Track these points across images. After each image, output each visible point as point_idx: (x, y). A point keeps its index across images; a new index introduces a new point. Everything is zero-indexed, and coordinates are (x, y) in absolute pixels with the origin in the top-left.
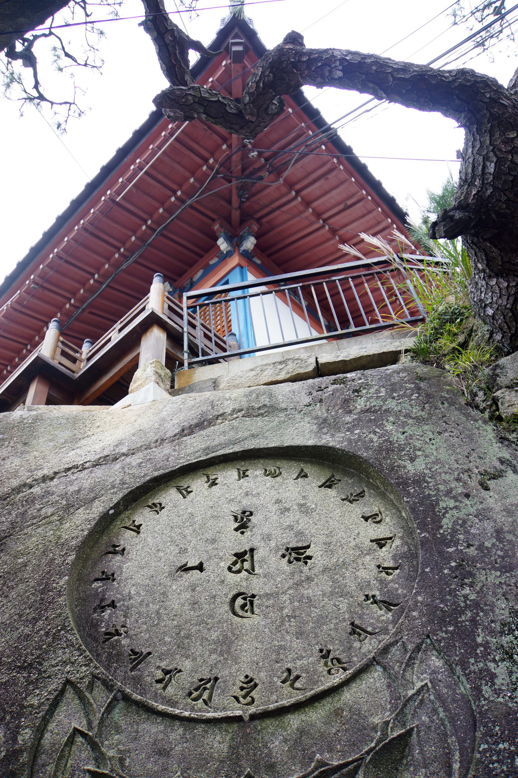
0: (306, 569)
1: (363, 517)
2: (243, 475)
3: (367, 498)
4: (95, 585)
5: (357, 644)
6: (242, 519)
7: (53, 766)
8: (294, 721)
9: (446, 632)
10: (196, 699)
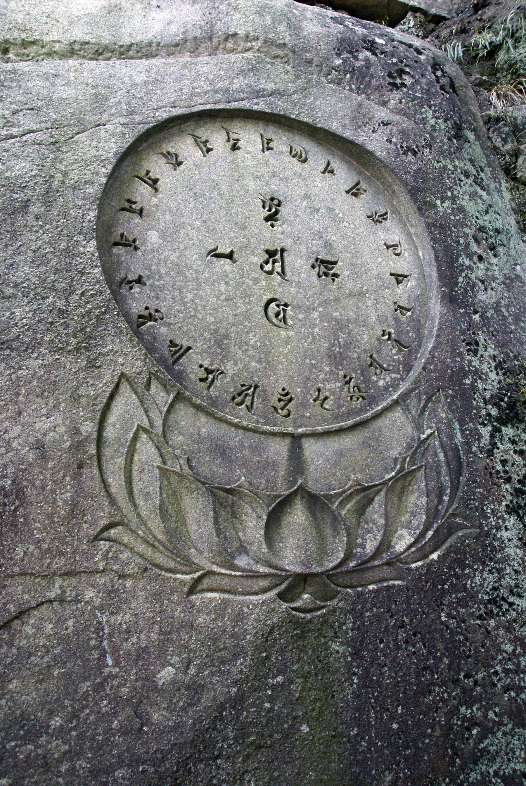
3: (388, 223)
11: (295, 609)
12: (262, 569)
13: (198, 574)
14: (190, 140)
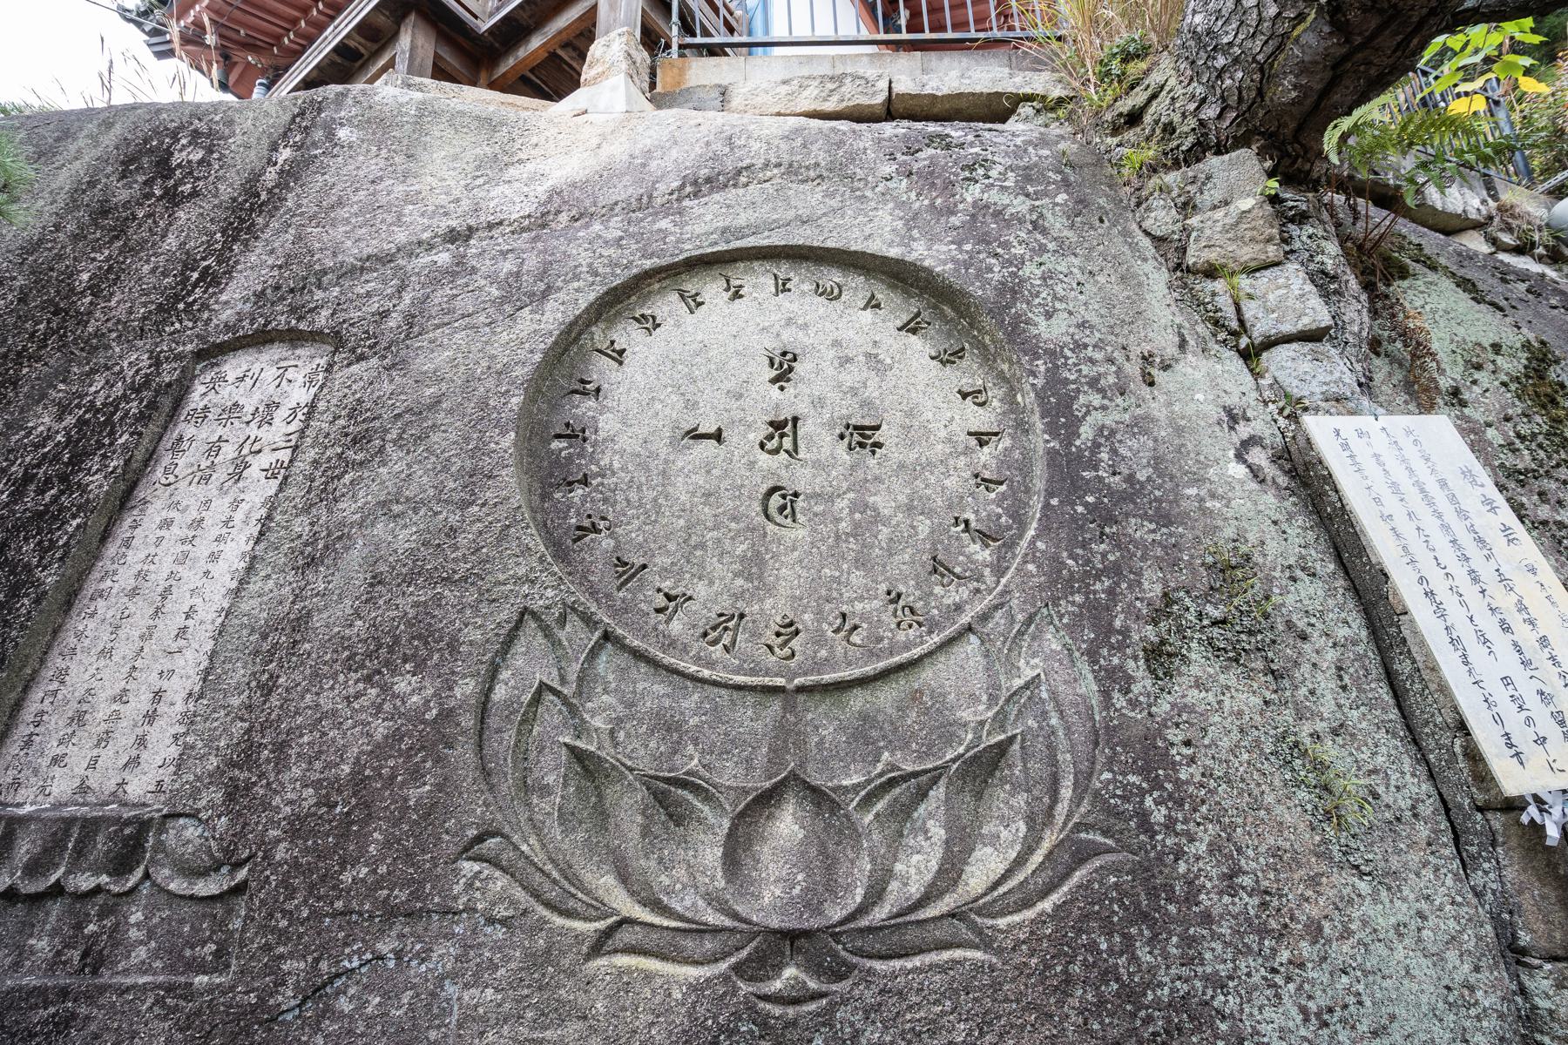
0: (872, 462)
1: (959, 392)
2: (782, 287)
3: (965, 363)
4: (556, 445)
5: (938, 590)
6: (781, 365)
7: (513, 732)
8: (858, 701)
9: (1073, 603)
10: (714, 643)
11: (766, 998)
12: (712, 918)
13: (610, 921)
14: (674, 297)
